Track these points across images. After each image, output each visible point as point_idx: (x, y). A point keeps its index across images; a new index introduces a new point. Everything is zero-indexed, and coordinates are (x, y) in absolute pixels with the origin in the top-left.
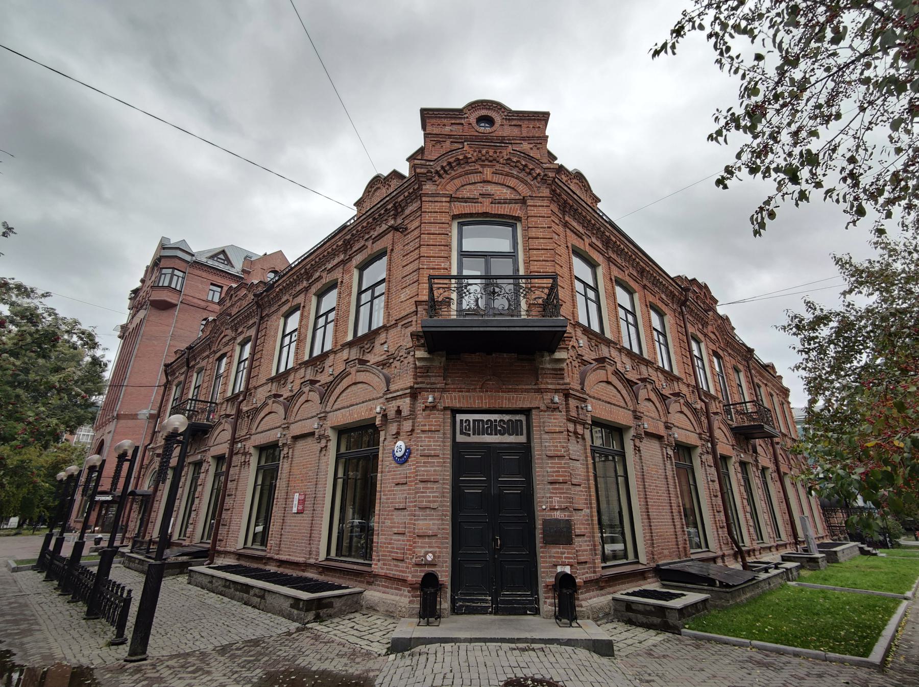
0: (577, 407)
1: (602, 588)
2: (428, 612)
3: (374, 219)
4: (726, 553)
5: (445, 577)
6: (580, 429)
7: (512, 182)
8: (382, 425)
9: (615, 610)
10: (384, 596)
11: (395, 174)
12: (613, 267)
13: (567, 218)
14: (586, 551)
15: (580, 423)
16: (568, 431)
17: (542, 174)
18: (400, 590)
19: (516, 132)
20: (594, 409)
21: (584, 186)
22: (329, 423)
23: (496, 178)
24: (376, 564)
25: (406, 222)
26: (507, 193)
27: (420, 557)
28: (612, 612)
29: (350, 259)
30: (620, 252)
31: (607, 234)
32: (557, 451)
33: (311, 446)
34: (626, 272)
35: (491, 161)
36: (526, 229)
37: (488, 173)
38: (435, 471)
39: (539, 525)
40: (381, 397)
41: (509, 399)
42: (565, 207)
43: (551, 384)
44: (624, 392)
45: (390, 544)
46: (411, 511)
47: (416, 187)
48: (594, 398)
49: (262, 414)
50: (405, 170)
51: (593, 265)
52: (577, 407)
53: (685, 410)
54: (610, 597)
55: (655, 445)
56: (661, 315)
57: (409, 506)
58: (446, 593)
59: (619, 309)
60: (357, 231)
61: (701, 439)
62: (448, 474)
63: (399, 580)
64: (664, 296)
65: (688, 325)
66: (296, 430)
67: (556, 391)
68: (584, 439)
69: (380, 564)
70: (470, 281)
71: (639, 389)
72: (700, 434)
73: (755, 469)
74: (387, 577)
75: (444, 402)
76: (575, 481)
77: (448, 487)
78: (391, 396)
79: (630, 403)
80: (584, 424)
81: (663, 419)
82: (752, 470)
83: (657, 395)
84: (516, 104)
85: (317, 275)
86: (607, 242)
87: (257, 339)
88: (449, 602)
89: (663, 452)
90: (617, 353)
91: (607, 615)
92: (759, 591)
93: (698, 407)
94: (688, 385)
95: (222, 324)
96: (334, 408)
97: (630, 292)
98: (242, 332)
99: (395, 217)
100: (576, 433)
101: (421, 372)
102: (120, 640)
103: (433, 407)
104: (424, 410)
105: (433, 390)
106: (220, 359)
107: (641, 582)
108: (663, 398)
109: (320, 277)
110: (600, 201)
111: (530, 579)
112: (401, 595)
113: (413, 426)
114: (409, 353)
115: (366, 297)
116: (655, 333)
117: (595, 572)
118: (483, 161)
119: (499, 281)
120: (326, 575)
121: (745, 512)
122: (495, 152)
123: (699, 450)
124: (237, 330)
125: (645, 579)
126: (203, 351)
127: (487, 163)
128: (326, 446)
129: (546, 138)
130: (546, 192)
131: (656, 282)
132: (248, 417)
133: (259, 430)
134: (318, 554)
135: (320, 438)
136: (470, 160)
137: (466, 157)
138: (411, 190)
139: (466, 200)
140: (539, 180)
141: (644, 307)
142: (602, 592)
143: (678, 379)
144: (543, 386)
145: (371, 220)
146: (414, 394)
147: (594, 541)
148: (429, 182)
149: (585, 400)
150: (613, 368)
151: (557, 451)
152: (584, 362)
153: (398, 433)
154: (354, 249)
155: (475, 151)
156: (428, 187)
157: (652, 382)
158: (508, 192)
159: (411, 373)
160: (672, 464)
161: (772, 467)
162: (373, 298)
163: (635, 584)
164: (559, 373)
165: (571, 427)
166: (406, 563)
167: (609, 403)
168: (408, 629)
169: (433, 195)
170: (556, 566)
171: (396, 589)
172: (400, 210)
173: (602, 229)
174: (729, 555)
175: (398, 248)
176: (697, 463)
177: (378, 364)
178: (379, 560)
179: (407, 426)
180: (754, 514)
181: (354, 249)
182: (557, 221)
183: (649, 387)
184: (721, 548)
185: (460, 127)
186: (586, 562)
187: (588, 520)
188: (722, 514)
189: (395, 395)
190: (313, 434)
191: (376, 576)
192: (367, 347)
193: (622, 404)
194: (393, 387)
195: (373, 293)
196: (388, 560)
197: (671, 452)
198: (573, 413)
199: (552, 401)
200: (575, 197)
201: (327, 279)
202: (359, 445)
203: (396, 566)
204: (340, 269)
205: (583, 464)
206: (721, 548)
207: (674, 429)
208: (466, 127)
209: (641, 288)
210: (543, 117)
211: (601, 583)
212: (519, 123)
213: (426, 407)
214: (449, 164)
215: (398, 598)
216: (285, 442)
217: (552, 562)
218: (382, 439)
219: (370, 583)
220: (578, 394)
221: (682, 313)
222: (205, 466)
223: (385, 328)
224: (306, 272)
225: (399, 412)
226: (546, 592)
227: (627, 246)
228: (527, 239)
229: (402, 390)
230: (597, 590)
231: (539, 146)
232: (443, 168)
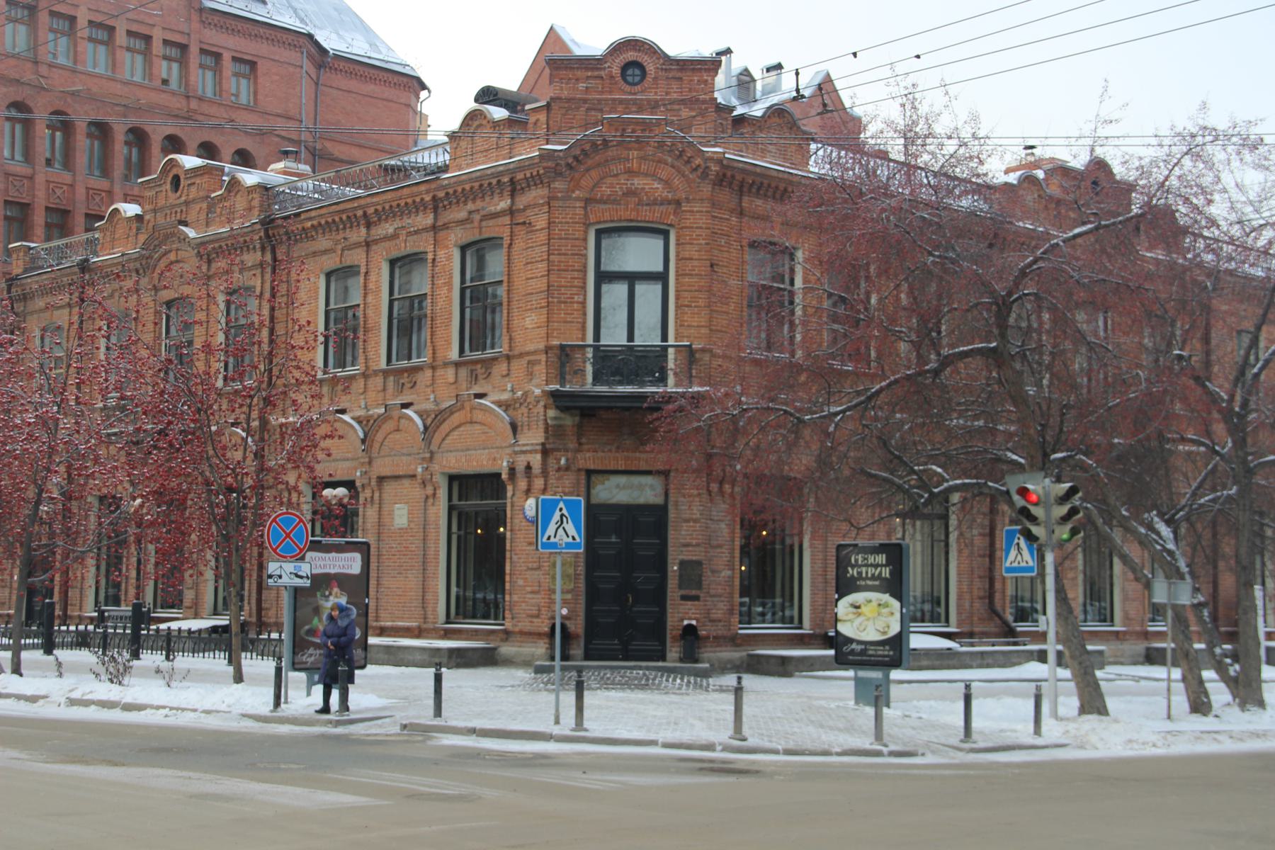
22: (435, 467)
39: (1170, 620)
54: (744, 654)
63: (530, 634)
74: (522, 633)
76: (715, 543)
84: (675, 47)
101: (554, 432)
105: (566, 450)
111: (657, 631)
128: (434, 495)
159: (541, 430)
190: (414, 476)
212: (679, 75)
216: (366, 481)
217: (680, 614)
218: (509, 494)
225: (529, 467)
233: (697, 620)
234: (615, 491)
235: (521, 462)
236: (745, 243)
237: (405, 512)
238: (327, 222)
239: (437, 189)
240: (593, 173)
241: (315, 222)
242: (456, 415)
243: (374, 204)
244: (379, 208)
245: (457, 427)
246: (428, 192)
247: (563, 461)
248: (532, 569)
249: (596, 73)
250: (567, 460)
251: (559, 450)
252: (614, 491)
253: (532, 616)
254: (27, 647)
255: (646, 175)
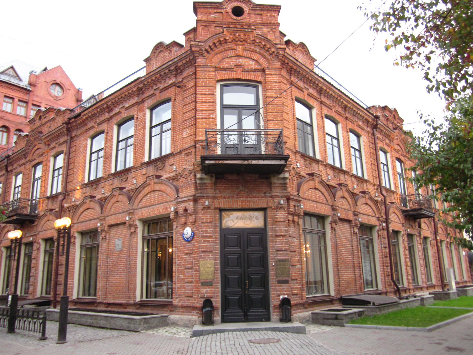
0: (295, 206)
1: (306, 308)
2: (208, 320)
3: (161, 75)
4: (388, 290)
5: (217, 302)
6: (296, 219)
7: (256, 56)
8: (175, 218)
9: (313, 319)
10: (182, 316)
11: (175, 44)
12: (324, 108)
13: (293, 78)
14: (297, 288)
15: (296, 215)
16: (289, 220)
17: (276, 52)
18: (191, 312)
19: (259, 19)
20: (305, 206)
21: (306, 51)
23: (245, 54)
24: (175, 300)
25: (185, 81)
26: (252, 64)
27: (203, 293)
28: (311, 320)
29: (143, 101)
30: (329, 96)
31: (320, 85)
32: (282, 232)
33: (124, 231)
34: (333, 110)
35: (242, 42)
36: (265, 90)
37: (240, 48)
38: (210, 245)
40: (173, 201)
41: (254, 202)
42: (291, 71)
43: (279, 193)
44: (326, 194)
45: (184, 288)
46: (196, 269)
47: (191, 58)
48: (306, 199)
49: (82, 210)
50: (182, 40)
51: (310, 108)
52: (295, 206)
53: (369, 202)
54: (310, 312)
55: (346, 226)
56: (358, 136)
57: (195, 266)
58: (218, 312)
59: (327, 136)
60: (148, 82)
61: (379, 220)
62: (218, 248)
63: (190, 307)
64: (361, 123)
65: (378, 141)
66: (112, 220)
67: (282, 197)
68: (298, 224)
69: (177, 300)
70: (231, 133)
71: (336, 191)
72: (378, 218)
73: (418, 239)
74: (182, 307)
75: (215, 205)
76: (292, 249)
77: (218, 254)
78: (180, 200)
79: (329, 201)
80: (299, 216)
81: (353, 209)
82: (417, 241)
83: (349, 194)
85: (117, 110)
86: (320, 91)
87: (70, 153)
88: (220, 316)
89: (351, 231)
90: (324, 168)
91: (308, 321)
92: (399, 308)
93: (380, 199)
94: (374, 185)
95: (35, 139)
96: (140, 206)
97: (336, 122)
98: (54, 147)
99: (176, 76)
100: (294, 221)
102: (43, 338)
103: (208, 208)
104: (202, 210)
105: (208, 197)
106: (35, 166)
107: (331, 306)
108: (353, 195)
109: (119, 113)
110: (316, 60)
111: (265, 302)
112: (192, 315)
113: (195, 219)
114: (191, 173)
115: (156, 131)
116: (352, 150)
117: (302, 299)
118: (237, 41)
119: (248, 133)
120: (142, 309)
121: (407, 266)
122: (245, 35)
123: (377, 228)
124: (49, 145)
125: (333, 304)
126: (19, 159)
127: (239, 42)
128: (135, 231)
129: (278, 24)
130: (278, 64)
131: (355, 114)
132: (69, 211)
133: (80, 220)
134: (135, 297)
135: (130, 226)
136: (228, 41)
137: (225, 39)
138: (188, 60)
139: (225, 69)
140: (274, 56)
141: (345, 133)
142: (306, 310)
143: (367, 181)
144: (274, 194)
145: (158, 76)
146: (195, 200)
147: (302, 283)
148: (201, 57)
149: (299, 201)
150: (319, 179)
151: (282, 232)
152: (301, 177)
153: (185, 223)
154: (146, 95)
155: (231, 34)
156: (200, 61)
157: (346, 186)
158: (253, 63)
159: (193, 186)
160: (357, 238)
161: (431, 236)
162: (162, 132)
163: (327, 306)
164: (284, 186)
165: (291, 218)
166: (194, 298)
167: (315, 202)
168: (198, 327)
169: (204, 66)
170: (279, 296)
171: (188, 312)
172: (179, 71)
173: (317, 82)
174: (390, 292)
175: (179, 98)
176: (375, 236)
177: (169, 179)
178: (177, 298)
179: (192, 218)
180: (413, 267)
181: (146, 95)
182: (285, 82)
183: (344, 189)
184: (386, 288)
185: (220, 15)
186: (297, 294)
187: (299, 271)
188: (389, 268)
189: (183, 199)
190: (125, 223)
191: (176, 307)
192: (159, 166)
193: (324, 201)
194: (181, 195)
195: (162, 128)
196: (183, 297)
197: (356, 230)
198: (292, 210)
199: (279, 203)
200: (298, 63)
201: (125, 115)
202: (158, 229)
203: (188, 300)
204: (135, 108)
205: (297, 239)
206: (386, 288)
207: (360, 216)
208: (225, 15)
209: (343, 119)
210: (277, 9)
211: (305, 305)
212: (260, 13)
213: (204, 208)
214: (214, 44)
215: (190, 317)
216: (103, 228)
217: (277, 294)
218: (174, 227)
219: (171, 311)
220: (296, 198)
221: (373, 134)
222: (35, 246)
223: (171, 155)
224: (108, 107)
225: (186, 210)
226: (274, 309)
227: (334, 92)
228: (265, 97)
229: (187, 197)
230: (303, 309)
231: (274, 30)
232: (210, 47)
233: (288, 295)
234: (236, 221)
235: (181, 207)
236: (294, 97)
237: (120, 242)
238: (92, 115)
239: (139, 83)
240: (219, 56)
241: (87, 116)
242: (147, 188)
243: (110, 100)
244: (113, 101)
245: (146, 195)
246: (135, 86)
247: (207, 203)
248: (188, 268)
249: (219, 11)
250: (209, 203)
251: (203, 197)
252: (235, 221)
253: (188, 297)
254: (18, 314)
255: (246, 57)
